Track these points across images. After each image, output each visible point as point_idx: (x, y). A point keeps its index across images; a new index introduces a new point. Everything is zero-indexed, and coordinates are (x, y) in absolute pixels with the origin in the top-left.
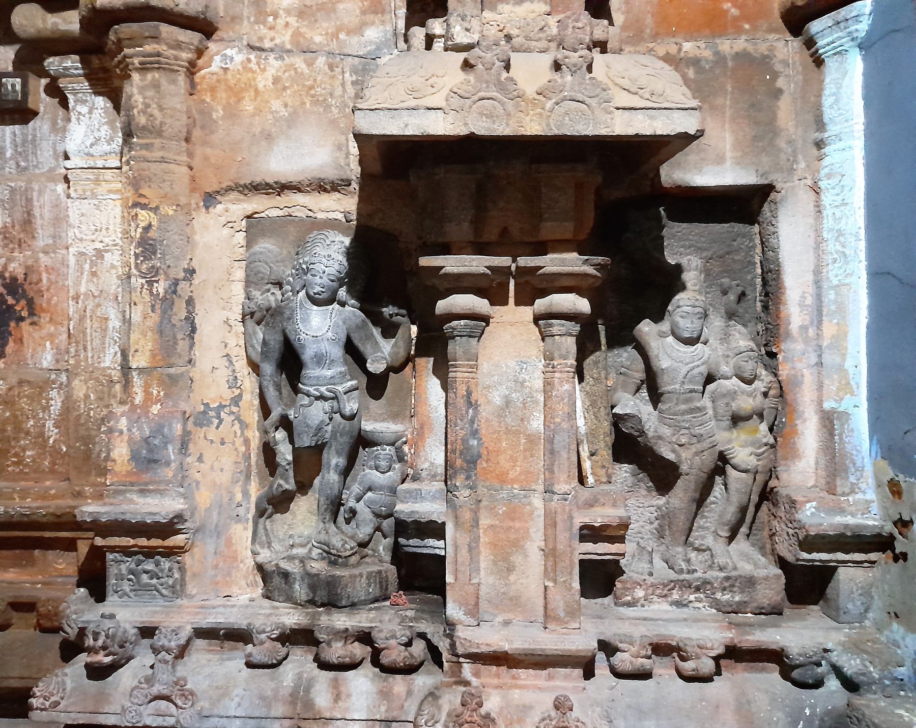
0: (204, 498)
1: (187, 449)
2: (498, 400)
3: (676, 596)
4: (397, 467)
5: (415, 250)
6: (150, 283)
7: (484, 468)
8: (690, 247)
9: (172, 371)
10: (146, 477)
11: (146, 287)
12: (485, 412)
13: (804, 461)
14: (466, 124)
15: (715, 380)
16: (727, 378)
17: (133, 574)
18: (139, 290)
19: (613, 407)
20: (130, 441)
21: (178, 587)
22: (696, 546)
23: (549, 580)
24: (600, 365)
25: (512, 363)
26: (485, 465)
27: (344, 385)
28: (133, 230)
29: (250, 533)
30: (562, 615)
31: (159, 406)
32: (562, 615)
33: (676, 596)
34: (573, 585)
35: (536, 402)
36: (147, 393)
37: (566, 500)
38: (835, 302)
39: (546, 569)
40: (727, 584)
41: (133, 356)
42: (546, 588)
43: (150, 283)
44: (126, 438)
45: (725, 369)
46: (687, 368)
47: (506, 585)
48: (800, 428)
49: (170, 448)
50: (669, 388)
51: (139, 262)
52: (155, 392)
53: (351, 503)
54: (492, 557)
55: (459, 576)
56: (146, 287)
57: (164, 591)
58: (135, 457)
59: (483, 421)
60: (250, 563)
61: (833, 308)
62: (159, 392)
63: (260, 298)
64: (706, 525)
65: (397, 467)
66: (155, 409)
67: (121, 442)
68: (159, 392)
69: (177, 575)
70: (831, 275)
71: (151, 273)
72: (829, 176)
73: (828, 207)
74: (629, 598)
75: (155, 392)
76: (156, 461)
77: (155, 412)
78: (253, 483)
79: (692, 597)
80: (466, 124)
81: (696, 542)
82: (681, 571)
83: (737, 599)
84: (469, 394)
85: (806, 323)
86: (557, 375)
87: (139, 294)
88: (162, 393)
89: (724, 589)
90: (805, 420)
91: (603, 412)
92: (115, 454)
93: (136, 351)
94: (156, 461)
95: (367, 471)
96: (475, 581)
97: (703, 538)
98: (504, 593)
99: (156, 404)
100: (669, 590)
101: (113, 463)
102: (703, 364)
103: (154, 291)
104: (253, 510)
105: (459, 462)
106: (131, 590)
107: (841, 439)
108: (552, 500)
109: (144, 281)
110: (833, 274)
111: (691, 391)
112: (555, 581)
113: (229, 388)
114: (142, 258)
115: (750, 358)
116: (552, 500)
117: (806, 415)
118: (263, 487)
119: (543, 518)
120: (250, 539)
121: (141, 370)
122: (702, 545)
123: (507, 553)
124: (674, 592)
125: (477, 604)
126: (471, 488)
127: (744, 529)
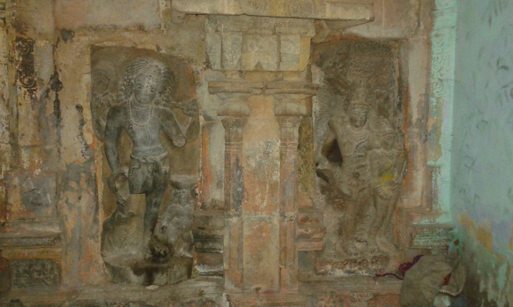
0: (71, 224)
1: (59, 195)
2: (253, 164)
3: (348, 268)
4: (192, 201)
5: (201, 70)
6: (31, 92)
7: (246, 203)
8: (360, 71)
9: (192, 237)
10: (32, 215)
11: (27, 93)
12: (246, 170)
13: (416, 193)
14: (241, 8)
15: (372, 149)
16: (378, 148)
17: (28, 273)
18: (23, 95)
19: (317, 165)
20: (22, 192)
21: (58, 280)
22: (359, 239)
23: (282, 265)
24: (310, 140)
25: (262, 143)
26: (246, 202)
27: (160, 156)
28: (17, 56)
29: (99, 244)
30: (289, 283)
31: (40, 170)
32: (289, 283)
33: (348, 268)
34: (295, 267)
35: (276, 165)
36: (32, 162)
37: (292, 220)
38: (436, 107)
39: (280, 259)
40: (374, 260)
41: (21, 138)
42: (280, 269)
43: (31, 92)
44: (18, 189)
45: (377, 143)
46: (357, 143)
47: (258, 268)
48: (415, 174)
49: (48, 196)
50: (348, 154)
51: (22, 77)
52: (37, 161)
53: (164, 223)
54: (250, 253)
55: (231, 265)
56: (27, 93)
57: (49, 283)
58: (24, 201)
59: (245, 176)
60: (101, 262)
61: (435, 110)
62: (39, 161)
63: (102, 98)
64: (364, 228)
65: (192, 201)
66: (38, 172)
67: (15, 192)
68: (39, 161)
69: (56, 273)
70: (435, 91)
71: (31, 84)
72: (437, 36)
73: (435, 53)
74: (323, 270)
75: (37, 161)
76: (39, 204)
77: (37, 174)
78: (100, 214)
79: (356, 268)
80: (241, 8)
81: (359, 237)
82: (351, 254)
83: (380, 267)
84: (238, 160)
85: (420, 117)
86: (288, 150)
87: (23, 98)
88: (41, 162)
89: (373, 263)
90: (417, 171)
91: (311, 167)
92: (11, 201)
93: (23, 135)
94: (39, 204)
95: (174, 205)
96: (241, 267)
97: (362, 235)
98: (256, 273)
99: (38, 169)
100: (345, 265)
101: (10, 207)
102: (366, 140)
103: (34, 96)
104: (101, 229)
105: (232, 201)
106: (27, 283)
107: (435, 182)
108: (284, 221)
109: (26, 90)
110: (436, 90)
111: (360, 156)
112: (285, 266)
113: (83, 156)
114: (24, 75)
115: (391, 137)
116: (284, 221)
117: (418, 167)
118: (107, 216)
119: (278, 231)
120: (100, 248)
121: (27, 147)
122: (362, 239)
123: (259, 251)
124: (347, 266)
125: (242, 281)
126: (239, 216)
127: (383, 228)
